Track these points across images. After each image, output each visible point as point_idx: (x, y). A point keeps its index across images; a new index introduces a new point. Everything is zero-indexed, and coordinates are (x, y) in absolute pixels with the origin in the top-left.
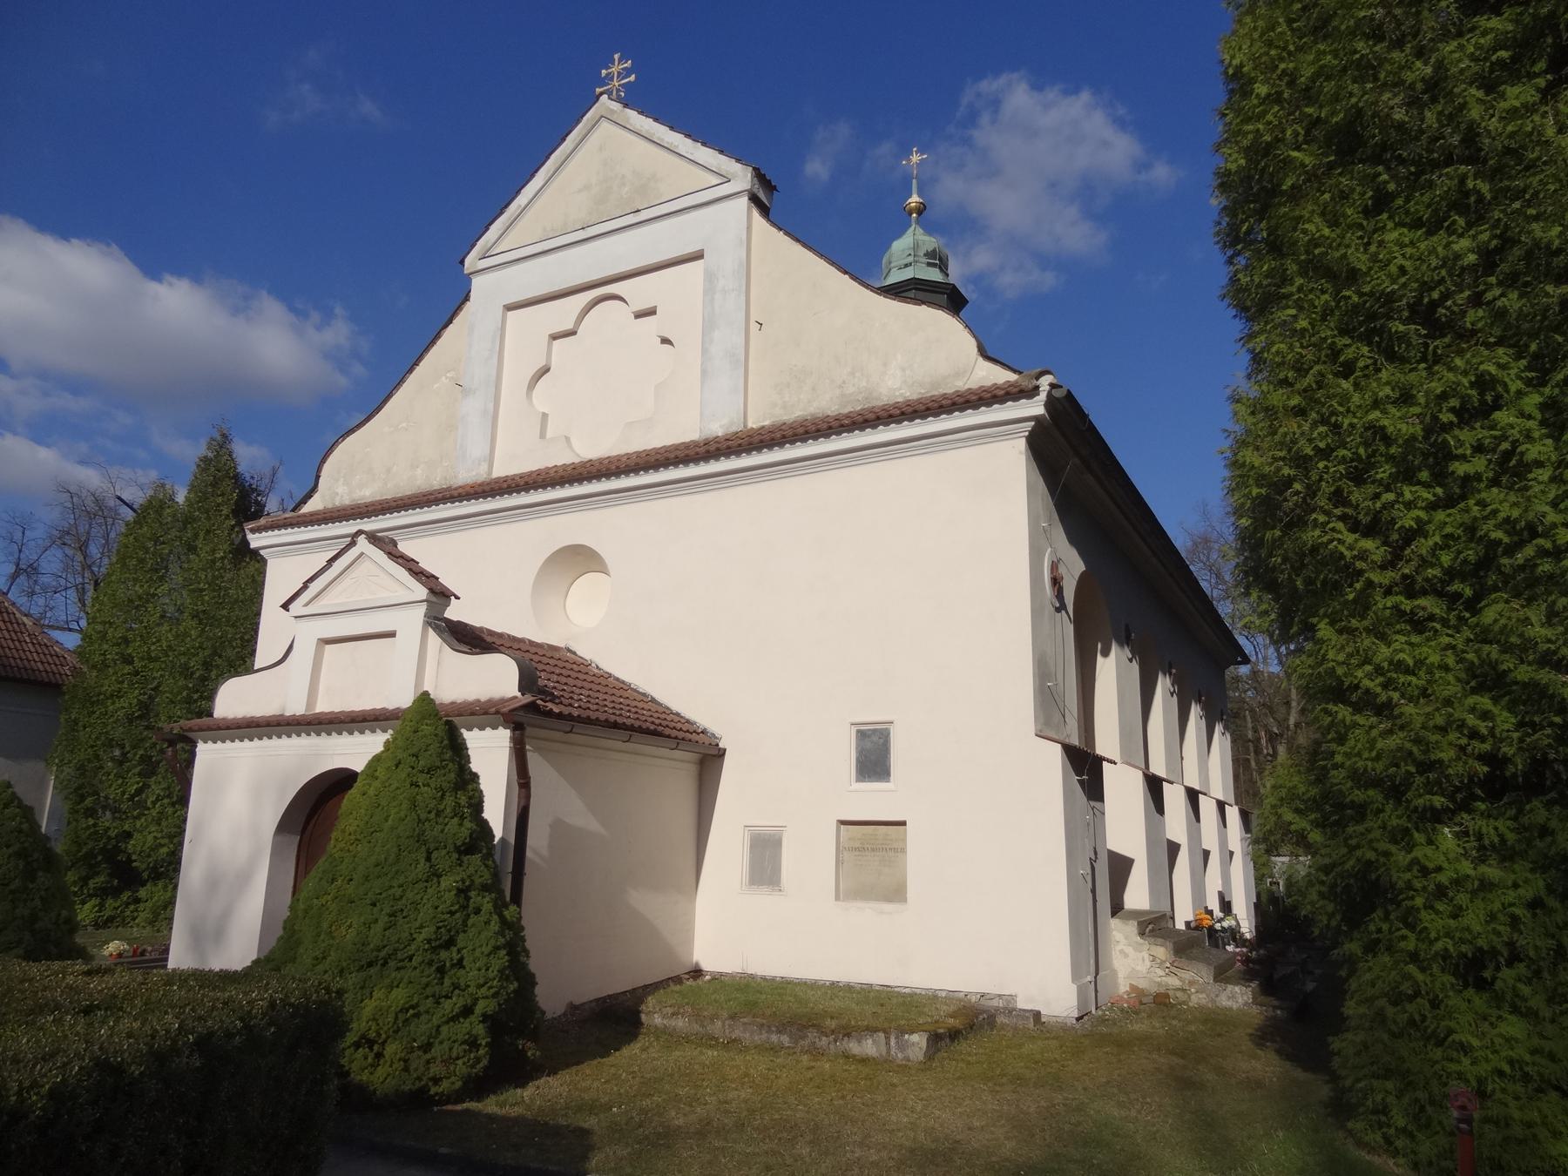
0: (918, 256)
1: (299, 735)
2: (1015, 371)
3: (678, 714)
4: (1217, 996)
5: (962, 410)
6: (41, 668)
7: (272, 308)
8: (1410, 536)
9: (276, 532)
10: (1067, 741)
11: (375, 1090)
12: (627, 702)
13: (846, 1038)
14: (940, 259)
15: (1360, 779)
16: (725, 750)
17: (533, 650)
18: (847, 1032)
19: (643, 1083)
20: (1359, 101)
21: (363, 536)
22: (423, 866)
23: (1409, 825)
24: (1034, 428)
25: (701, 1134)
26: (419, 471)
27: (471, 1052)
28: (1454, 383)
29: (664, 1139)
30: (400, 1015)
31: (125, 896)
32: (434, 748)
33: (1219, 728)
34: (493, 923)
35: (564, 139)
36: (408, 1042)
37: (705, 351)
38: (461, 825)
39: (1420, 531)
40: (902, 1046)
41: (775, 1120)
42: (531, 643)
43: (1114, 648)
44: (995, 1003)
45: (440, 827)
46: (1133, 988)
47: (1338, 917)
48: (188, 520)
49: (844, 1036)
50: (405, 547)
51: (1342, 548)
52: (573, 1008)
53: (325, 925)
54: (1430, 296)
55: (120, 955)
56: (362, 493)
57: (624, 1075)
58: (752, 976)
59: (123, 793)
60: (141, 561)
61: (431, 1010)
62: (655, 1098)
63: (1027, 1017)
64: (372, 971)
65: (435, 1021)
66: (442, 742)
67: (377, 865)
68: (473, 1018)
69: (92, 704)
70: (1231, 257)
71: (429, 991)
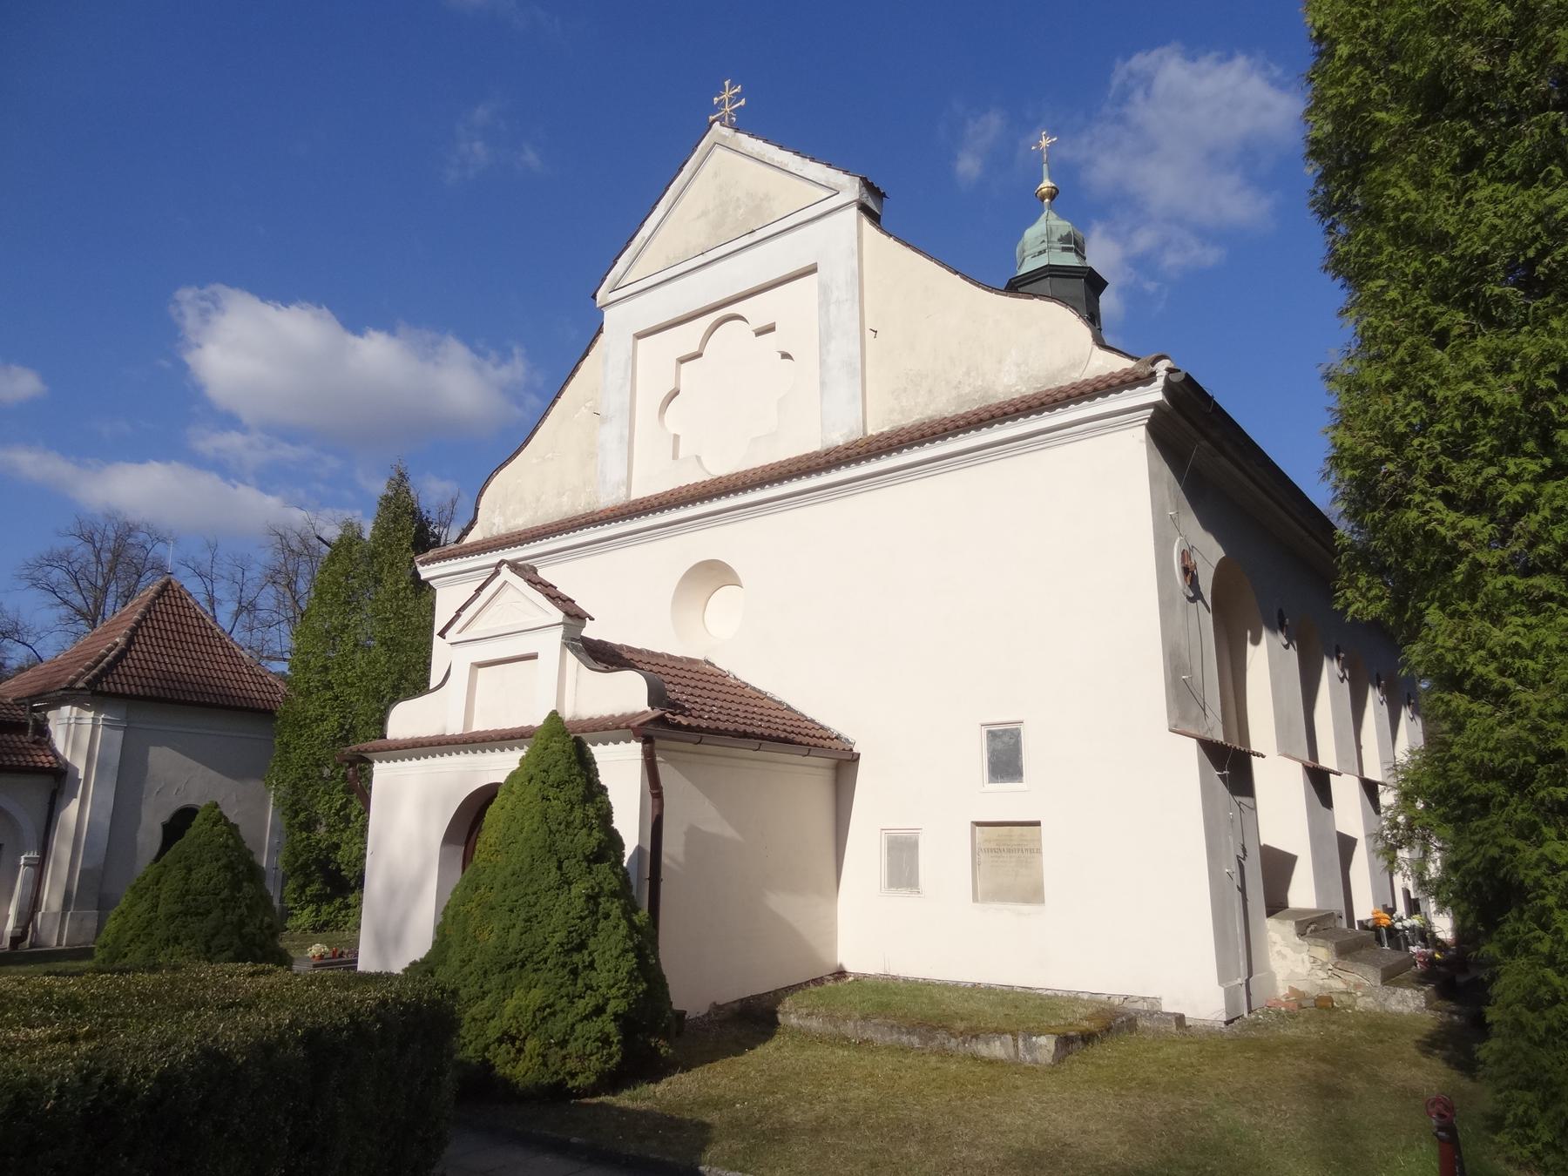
0: (1052, 242)
1: (502, 750)
2: (1132, 358)
3: (812, 721)
4: (1385, 1000)
5: (1077, 402)
6: (258, 697)
7: (456, 350)
8: (1517, 512)
9: (442, 563)
10: (1209, 736)
11: (518, 1082)
12: (761, 711)
13: (974, 1040)
15: (1479, 771)
16: (859, 755)
17: (671, 664)
18: (975, 1034)
19: (769, 1081)
20: (1439, 54)
21: (505, 565)
22: (554, 875)
23: (1537, 819)
25: (816, 1131)
26: (565, 499)
27: (603, 1048)
28: (1551, 346)
29: (781, 1134)
30: (537, 1013)
31: (338, 902)
32: (562, 765)
33: (1405, 714)
34: (621, 927)
35: (681, 170)
36: (546, 1039)
37: (822, 363)
38: (589, 835)
39: (1528, 505)
40: (1030, 1049)
41: (892, 1118)
42: (671, 658)
43: (1265, 635)
44: (1140, 1006)
45: (570, 838)
46: (1293, 991)
47: (1472, 917)
48: (374, 555)
49: (972, 1038)
50: (545, 574)
51: (1442, 530)
52: (716, 1008)
53: (470, 930)
54: (1525, 255)
55: (321, 957)
56: (516, 522)
57: (753, 1073)
58: (895, 978)
59: (330, 808)
60: (335, 595)
61: (566, 1009)
62: (778, 1096)
63: (1169, 1020)
64: (513, 972)
65: (570, 1020)
66: (570, 758)
67: (513, 875)
68: (604, 1017)
69: (301, 727)
70: (1332, 226)
71: (563, 991)
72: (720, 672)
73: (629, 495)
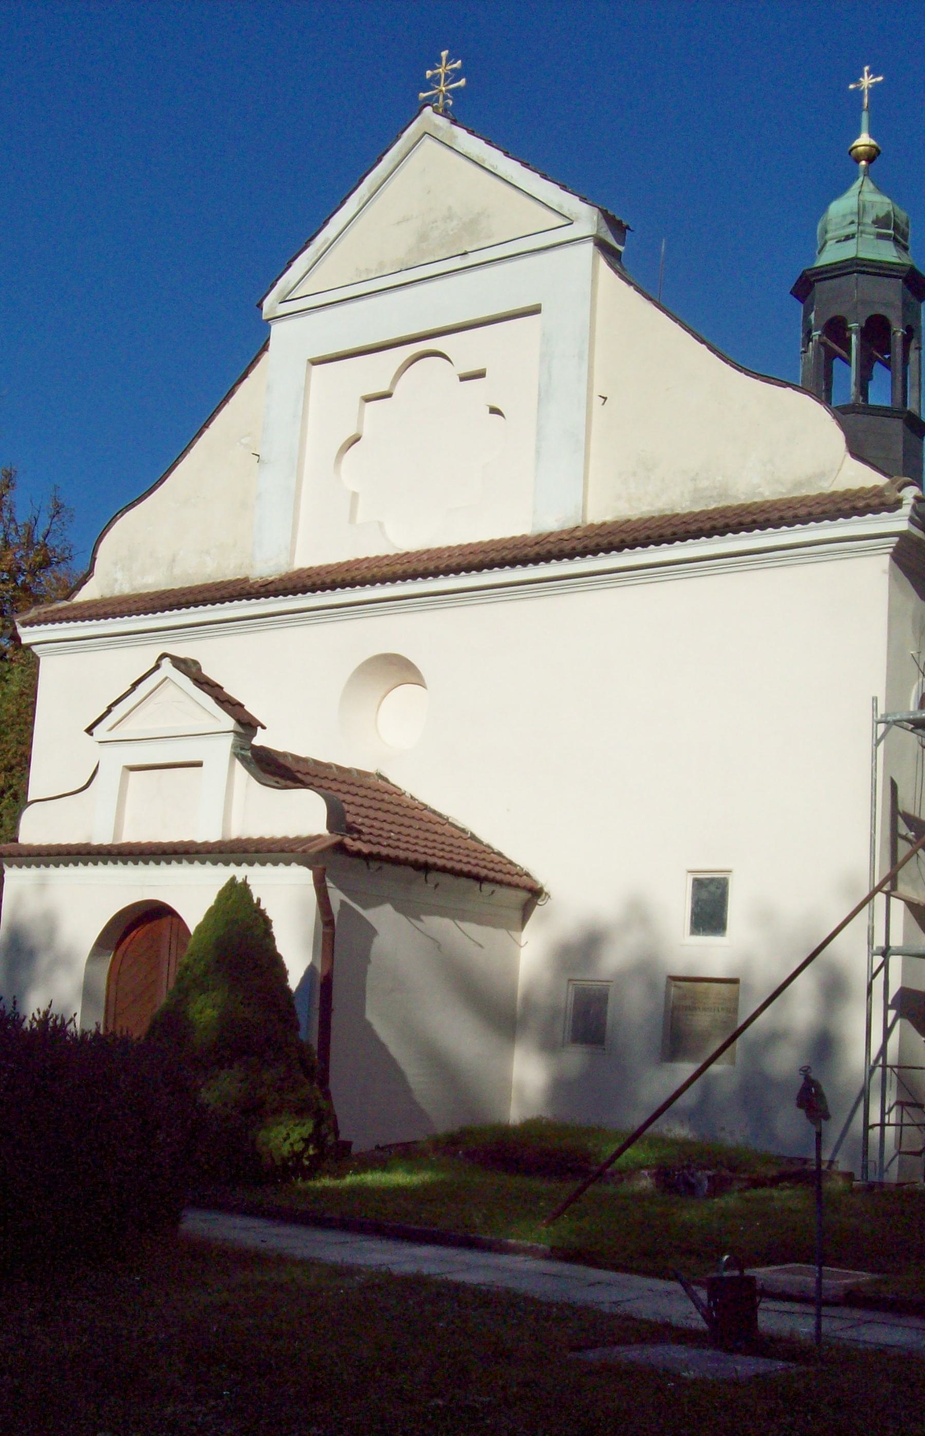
0: (864, 224)
3: (500, 854)
12: (443, 839)
14: (896, 228)
21: (167, 660)
24: (898, 544)
72: (395, 790)
73: (292, 563)
